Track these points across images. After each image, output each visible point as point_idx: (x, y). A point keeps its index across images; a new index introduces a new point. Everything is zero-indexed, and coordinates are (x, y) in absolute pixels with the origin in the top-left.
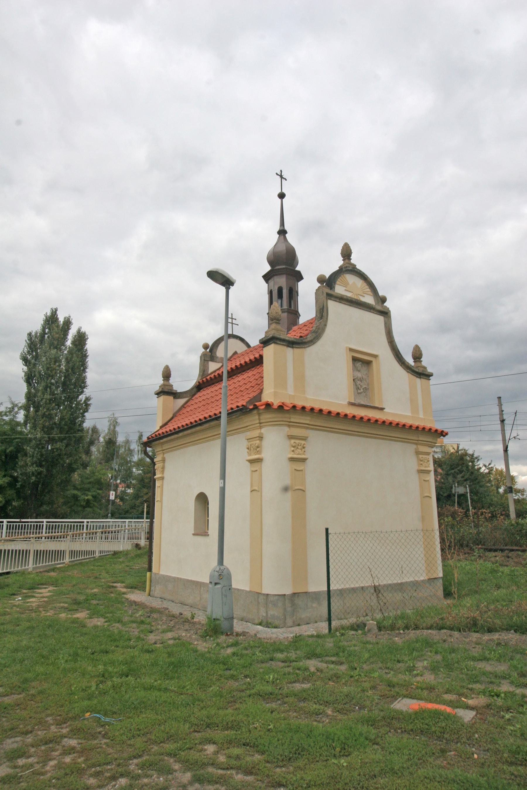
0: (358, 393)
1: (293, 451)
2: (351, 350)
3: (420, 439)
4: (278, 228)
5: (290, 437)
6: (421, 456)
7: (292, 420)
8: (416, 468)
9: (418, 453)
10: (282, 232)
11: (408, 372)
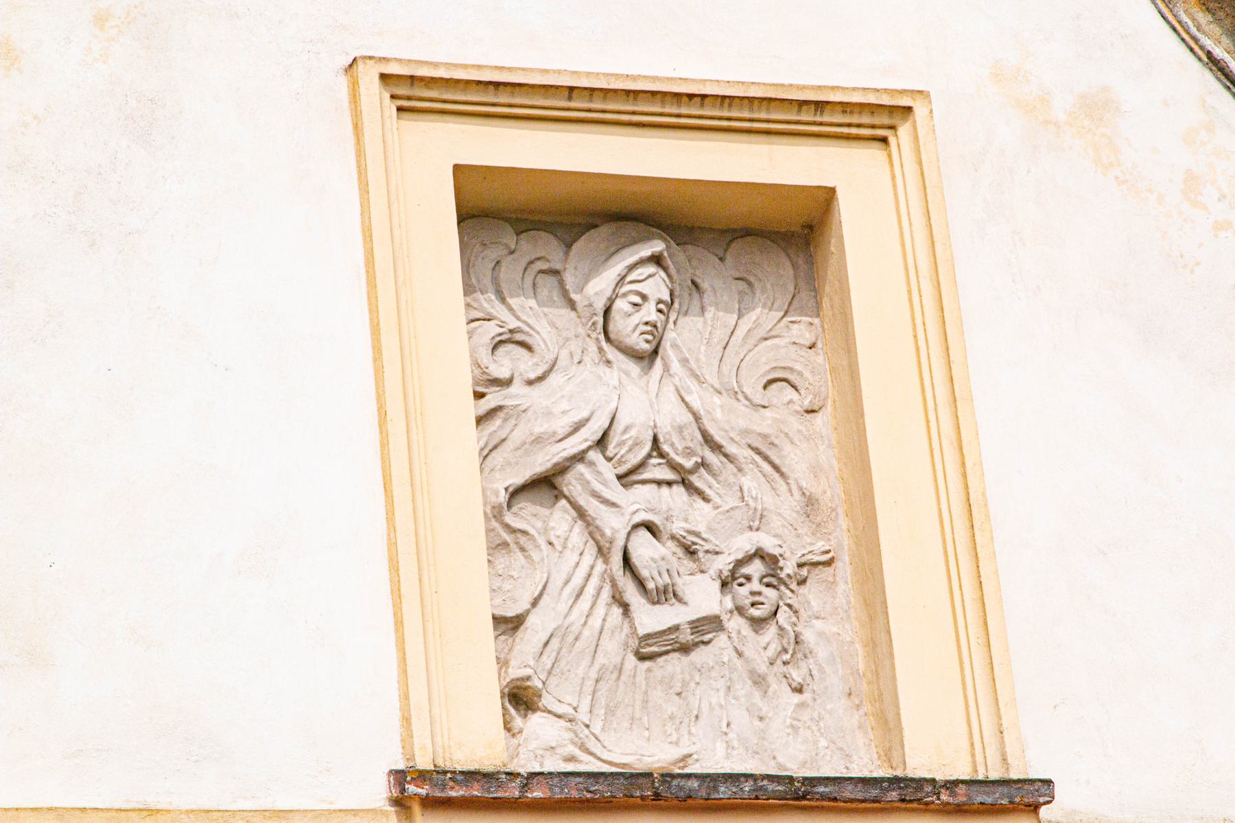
0: (649, 650)
2: (418, 94)
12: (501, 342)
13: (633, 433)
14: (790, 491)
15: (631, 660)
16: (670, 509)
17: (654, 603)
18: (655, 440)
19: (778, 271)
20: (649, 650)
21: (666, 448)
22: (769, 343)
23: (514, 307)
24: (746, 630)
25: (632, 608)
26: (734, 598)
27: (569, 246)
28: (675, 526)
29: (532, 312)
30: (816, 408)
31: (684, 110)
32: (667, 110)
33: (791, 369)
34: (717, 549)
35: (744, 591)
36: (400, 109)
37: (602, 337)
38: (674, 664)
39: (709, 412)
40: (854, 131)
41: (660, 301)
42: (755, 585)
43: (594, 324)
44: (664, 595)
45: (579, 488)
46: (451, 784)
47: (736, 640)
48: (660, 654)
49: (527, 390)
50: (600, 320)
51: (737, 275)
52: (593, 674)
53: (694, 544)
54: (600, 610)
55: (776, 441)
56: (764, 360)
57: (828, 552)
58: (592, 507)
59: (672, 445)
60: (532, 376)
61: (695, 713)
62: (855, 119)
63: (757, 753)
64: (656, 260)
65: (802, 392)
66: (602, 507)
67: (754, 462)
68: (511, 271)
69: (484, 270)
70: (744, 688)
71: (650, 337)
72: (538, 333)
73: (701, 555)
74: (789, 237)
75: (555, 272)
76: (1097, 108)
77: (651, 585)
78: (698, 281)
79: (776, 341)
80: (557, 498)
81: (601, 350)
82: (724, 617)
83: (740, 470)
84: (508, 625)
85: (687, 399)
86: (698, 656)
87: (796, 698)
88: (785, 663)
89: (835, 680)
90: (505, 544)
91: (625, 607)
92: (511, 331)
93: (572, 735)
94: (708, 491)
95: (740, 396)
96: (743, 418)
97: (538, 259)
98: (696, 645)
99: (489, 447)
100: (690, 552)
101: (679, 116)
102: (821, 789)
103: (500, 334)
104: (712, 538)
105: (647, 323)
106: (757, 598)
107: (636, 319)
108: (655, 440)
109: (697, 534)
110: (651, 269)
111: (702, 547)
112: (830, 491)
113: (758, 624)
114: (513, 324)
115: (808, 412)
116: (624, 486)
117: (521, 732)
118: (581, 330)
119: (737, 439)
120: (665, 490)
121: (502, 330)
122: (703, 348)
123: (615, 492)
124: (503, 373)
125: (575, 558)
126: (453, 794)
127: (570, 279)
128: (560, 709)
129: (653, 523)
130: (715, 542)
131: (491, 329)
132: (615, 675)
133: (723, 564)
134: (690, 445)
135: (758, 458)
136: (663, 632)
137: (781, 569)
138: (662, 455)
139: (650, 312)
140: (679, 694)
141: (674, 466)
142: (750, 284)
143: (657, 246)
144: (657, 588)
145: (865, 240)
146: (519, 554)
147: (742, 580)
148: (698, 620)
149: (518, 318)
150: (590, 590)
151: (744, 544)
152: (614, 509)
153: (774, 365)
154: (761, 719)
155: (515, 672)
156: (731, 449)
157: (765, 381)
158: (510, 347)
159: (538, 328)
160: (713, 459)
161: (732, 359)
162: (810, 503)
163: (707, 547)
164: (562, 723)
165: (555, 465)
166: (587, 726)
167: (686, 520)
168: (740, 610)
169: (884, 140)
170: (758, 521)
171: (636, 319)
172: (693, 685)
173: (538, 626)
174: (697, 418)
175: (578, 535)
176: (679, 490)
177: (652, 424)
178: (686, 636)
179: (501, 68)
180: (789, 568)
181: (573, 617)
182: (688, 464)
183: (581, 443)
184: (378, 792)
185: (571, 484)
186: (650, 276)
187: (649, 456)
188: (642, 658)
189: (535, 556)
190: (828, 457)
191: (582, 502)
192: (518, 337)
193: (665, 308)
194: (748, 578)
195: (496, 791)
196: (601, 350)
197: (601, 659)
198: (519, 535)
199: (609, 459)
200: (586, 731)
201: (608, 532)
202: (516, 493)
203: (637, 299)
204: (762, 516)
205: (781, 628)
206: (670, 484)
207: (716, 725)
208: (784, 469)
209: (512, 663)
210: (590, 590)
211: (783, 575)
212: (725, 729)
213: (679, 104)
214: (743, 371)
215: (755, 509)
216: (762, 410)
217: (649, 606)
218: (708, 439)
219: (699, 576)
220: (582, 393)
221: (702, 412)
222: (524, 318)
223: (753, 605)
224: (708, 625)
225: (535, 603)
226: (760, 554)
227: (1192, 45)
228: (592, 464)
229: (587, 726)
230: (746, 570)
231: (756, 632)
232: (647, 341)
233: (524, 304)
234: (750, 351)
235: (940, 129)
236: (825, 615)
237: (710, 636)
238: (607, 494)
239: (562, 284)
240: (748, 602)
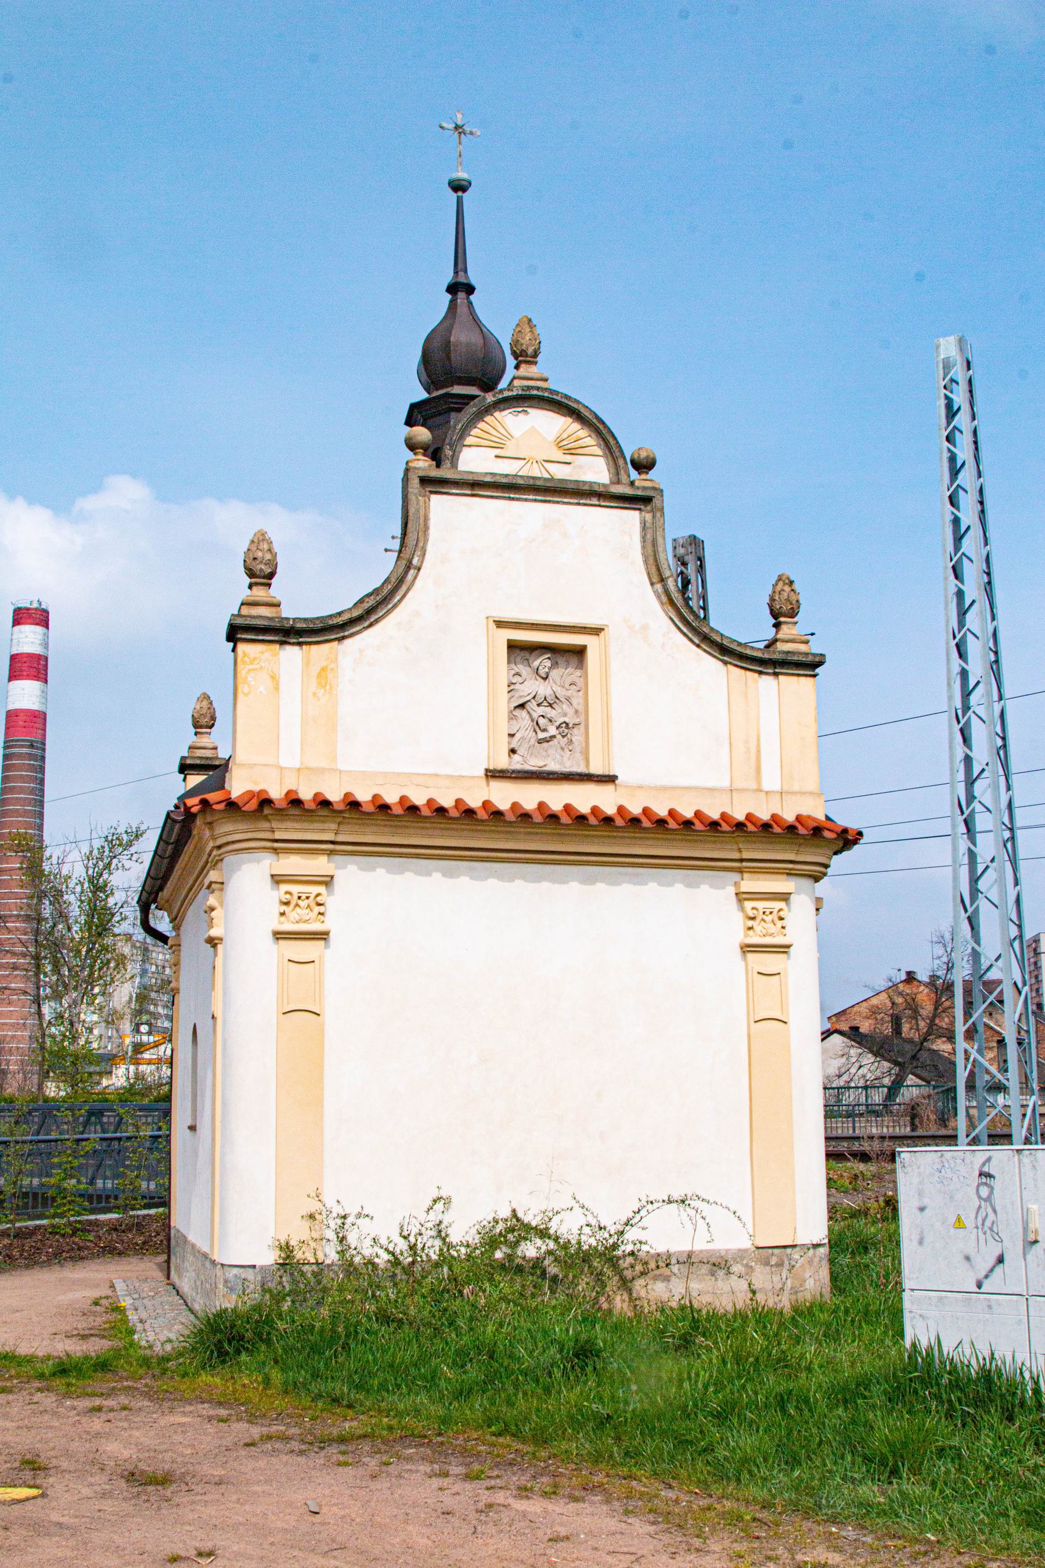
0: (540, 741)
1: (283, 914)
2: (500, 624)
3: (746, 855)
4: (448, 277)
5: (277, 880)
6: (748, 905)
7: (278, 835)
8: (739, 936)
9: (741, 897)
10: (460, 288)
11: (725, 663)
19: (574, 660)
20: (540, 741)
29: (522, 668)
38: (545, 745)
44: (544, 730)
68: (518, 659)
69: (512, 659)
70: (559, 750)
74: (579, 653)
76: (645, 628)
84: (511, 735)
89: (578, 749)
112: (581, 708)
113: (563, 737)
123: (536, 708)
131: (513, 672)
133: (557, 724)
139: (547, 670)
143: (549, 655)
145: (592, 657)
151: (562, 720)
155: (512, 746)
162: (577, 711)
170: (565, 715)
173: (518, 736)
175: (528, 717)
184: (482, 773)
185: (527, 706)
190: (581, 701)
193: (550, 669)
202: (516, 707)
220: (531, 687)
227: (667, 614)
233: (521, 666)
235: (610, 632)
236: (577, 735)
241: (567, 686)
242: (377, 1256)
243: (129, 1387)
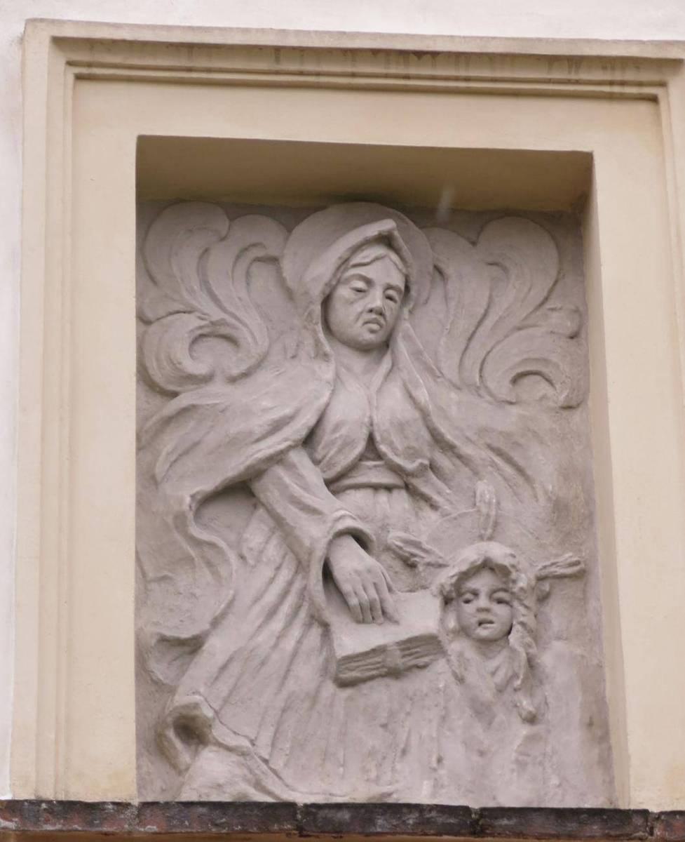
0: (349, 676)
2: (95, 59)
12: (202, 336)
13: (343, 431)
14: (536, 496)
15: (330, 688)
16: (386, 517)
17: (358, 622)
18: (371, 439)
20: (349, 676)
21: (383, 448)
22: (522, 332)
23: (221, 298)
24: (470, 652)
25: (333, 628)
26: (459, 619)
27: (290, 231)
28: (391, 535)
30: (573, 403)
31: (412, 71)
32: (393, 70)
33: (546, 361)
34: (441, 561)
35: (470, 609)
36: (79, 78)
37: (319, 328)
38: (381, 694)
39: (441, 409)
40: (616, 89)
41: (389, 287)
42: (483, 602)
43: (310, 314)
44: (371, 613)
45: (276, 493)
46: (46, 815)
47: (456, 663)
48: (364, 680)
49: (229, 389)
50: (317, 308)
51: (490, 260)
52: (280, 703)
53: (414, 555)
54: (296, 632)
55: (522, 441)
56: (514, 353)
57: (577, 563)
58: (291, 514)
59: (391, 445)
60: (235, 372)
61: (402, 746)
62: (618, 76)
63: (472, 792)
64: (386, 240)
65: (558, 386)
66: (303, 515)
67: (493, 464)
71: (375, 327)
72: (245, 325)
73: (421, 568)
75: (274, 260)
77: (353, 601)
78: (442, 266)
79: (531, 331)
80: (255, 506)
81: (317, 343)
82: (444, 638)
83: (476, 473)
85: (414, 393)
86: (417, 683)
87: (525, 730)
88: (515, 690)
90: (189, 560)
91: (326, 626)
92: (213, 323)
93: (246, 771)
94: (436, 497)
95: (482, 392)
96: (484, 414)
97: (254, 245)
98: (410, 669)
99: (179, 452)
100: (409, 564)
101: (407, 77)
102: (505, 822)
103: (201, 327)
104: (436, 550)
105: (371, 311)
106: (483, 616)
107: (358, 307)
108: (371, 439)
109: (417, 545)
110: (379, 250)
111: (422, 559)
114: (217, 315)
115: (569, 408)
116: (335, 493)
117: (187, 769)
118: (297, 322)
119: (474, 438)
120: (383, 497)
121: (203, 323)
122: (443, 341)
123: (322, 498)
124: (200, 369)
125: (269, 573)
126: (49, 828)
127: (288, 267)
128: (232, 741)
129: (361, 531)
130: (439, 553)
132: (307, 704)
133: (445, 577)
134: (414, 444)
135: (498, 460)
136: (366, 655)
137: (514, 582)
138: (379, 456)
139: (376, 299)
140: (384, 726)
141: (396, 470)
142: (505, 270)
143: (387, 225)
144: (361, 605)
146: (206, 571)
147: (468, 596)
148: (410, 640)
149: (224, 310)
150: (286, 608)
151: (471, 554)
152: (316, 517)
153: (525, 356)
154: (482, 753)
156: (467, 450)
157: (514, 373)
158: (213, 342)
159: (247, 321)
160: (444, 462)
161: (477, 351)
163: (428, 559)
164: (234, 758)
165: (249, 468)
166: (266, 761)
167: (406, 530)
168: (463, 631)
169: (654, 99)
170: (493, 529)
171: (358, 307)
172: (402, 715)
174: (425, 415)
176: (401, 498)
177: (366, 420)
178: (397, 660)
179: (191, 28)
180: (524, 581)
181: (260, 639)
182: (410, 466)
183: (279, 443)
185: (268, 490)
186: (377, 259)
187: (362, 458)
188: (343, 684)
189: (223, 571)
191: (280, 510)
192: (224, 330)
194: (476, 594)
195: (101, 824)
196: (317, 343)
197: (291, 685)
198: (206, 549)
199: (316, 462)
200: (264, 767)
201: (307, 543)
203: (361, 285)
204: (496, 524)
205: (513, 650)
206: (389, 488)
207: (432, 761)
208: (529, 472)
209: (181, 690)
210: (286, 608)
211: (516, 590)
212: (434, 764)
213: (407, 63)
214: (488, 368)
215: (488, 516)
216: (508, 407)
217: (354, 625)
218: (438, 440)
219: (419, 594)
220: (291, 391)
221: (431, 407)
222: (232, 309)
223: (480, 624)
224: (423, 648)
225: (215, 623)
226: (487, 565)
228: (291, 467)
229: (266, 761)
230: (474, 584)
231: (484, 654)
232: (372, 331)
234: (498, 342)
237: (426, 659)
238: (308, 499)
239: (279, 271)
240: (474, 620)
241: (498, 381)
242: (551, 372)
243: (344, 796)
